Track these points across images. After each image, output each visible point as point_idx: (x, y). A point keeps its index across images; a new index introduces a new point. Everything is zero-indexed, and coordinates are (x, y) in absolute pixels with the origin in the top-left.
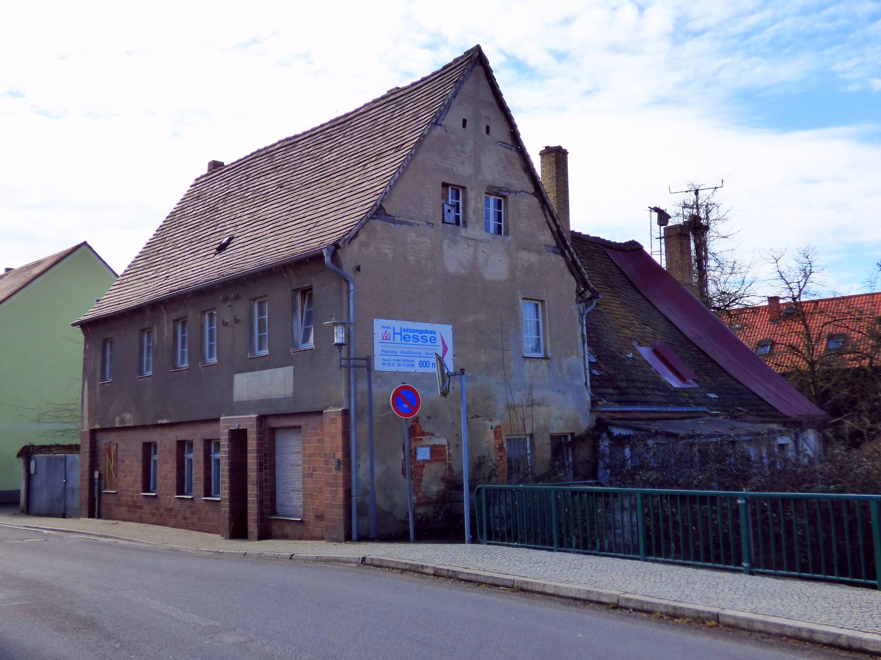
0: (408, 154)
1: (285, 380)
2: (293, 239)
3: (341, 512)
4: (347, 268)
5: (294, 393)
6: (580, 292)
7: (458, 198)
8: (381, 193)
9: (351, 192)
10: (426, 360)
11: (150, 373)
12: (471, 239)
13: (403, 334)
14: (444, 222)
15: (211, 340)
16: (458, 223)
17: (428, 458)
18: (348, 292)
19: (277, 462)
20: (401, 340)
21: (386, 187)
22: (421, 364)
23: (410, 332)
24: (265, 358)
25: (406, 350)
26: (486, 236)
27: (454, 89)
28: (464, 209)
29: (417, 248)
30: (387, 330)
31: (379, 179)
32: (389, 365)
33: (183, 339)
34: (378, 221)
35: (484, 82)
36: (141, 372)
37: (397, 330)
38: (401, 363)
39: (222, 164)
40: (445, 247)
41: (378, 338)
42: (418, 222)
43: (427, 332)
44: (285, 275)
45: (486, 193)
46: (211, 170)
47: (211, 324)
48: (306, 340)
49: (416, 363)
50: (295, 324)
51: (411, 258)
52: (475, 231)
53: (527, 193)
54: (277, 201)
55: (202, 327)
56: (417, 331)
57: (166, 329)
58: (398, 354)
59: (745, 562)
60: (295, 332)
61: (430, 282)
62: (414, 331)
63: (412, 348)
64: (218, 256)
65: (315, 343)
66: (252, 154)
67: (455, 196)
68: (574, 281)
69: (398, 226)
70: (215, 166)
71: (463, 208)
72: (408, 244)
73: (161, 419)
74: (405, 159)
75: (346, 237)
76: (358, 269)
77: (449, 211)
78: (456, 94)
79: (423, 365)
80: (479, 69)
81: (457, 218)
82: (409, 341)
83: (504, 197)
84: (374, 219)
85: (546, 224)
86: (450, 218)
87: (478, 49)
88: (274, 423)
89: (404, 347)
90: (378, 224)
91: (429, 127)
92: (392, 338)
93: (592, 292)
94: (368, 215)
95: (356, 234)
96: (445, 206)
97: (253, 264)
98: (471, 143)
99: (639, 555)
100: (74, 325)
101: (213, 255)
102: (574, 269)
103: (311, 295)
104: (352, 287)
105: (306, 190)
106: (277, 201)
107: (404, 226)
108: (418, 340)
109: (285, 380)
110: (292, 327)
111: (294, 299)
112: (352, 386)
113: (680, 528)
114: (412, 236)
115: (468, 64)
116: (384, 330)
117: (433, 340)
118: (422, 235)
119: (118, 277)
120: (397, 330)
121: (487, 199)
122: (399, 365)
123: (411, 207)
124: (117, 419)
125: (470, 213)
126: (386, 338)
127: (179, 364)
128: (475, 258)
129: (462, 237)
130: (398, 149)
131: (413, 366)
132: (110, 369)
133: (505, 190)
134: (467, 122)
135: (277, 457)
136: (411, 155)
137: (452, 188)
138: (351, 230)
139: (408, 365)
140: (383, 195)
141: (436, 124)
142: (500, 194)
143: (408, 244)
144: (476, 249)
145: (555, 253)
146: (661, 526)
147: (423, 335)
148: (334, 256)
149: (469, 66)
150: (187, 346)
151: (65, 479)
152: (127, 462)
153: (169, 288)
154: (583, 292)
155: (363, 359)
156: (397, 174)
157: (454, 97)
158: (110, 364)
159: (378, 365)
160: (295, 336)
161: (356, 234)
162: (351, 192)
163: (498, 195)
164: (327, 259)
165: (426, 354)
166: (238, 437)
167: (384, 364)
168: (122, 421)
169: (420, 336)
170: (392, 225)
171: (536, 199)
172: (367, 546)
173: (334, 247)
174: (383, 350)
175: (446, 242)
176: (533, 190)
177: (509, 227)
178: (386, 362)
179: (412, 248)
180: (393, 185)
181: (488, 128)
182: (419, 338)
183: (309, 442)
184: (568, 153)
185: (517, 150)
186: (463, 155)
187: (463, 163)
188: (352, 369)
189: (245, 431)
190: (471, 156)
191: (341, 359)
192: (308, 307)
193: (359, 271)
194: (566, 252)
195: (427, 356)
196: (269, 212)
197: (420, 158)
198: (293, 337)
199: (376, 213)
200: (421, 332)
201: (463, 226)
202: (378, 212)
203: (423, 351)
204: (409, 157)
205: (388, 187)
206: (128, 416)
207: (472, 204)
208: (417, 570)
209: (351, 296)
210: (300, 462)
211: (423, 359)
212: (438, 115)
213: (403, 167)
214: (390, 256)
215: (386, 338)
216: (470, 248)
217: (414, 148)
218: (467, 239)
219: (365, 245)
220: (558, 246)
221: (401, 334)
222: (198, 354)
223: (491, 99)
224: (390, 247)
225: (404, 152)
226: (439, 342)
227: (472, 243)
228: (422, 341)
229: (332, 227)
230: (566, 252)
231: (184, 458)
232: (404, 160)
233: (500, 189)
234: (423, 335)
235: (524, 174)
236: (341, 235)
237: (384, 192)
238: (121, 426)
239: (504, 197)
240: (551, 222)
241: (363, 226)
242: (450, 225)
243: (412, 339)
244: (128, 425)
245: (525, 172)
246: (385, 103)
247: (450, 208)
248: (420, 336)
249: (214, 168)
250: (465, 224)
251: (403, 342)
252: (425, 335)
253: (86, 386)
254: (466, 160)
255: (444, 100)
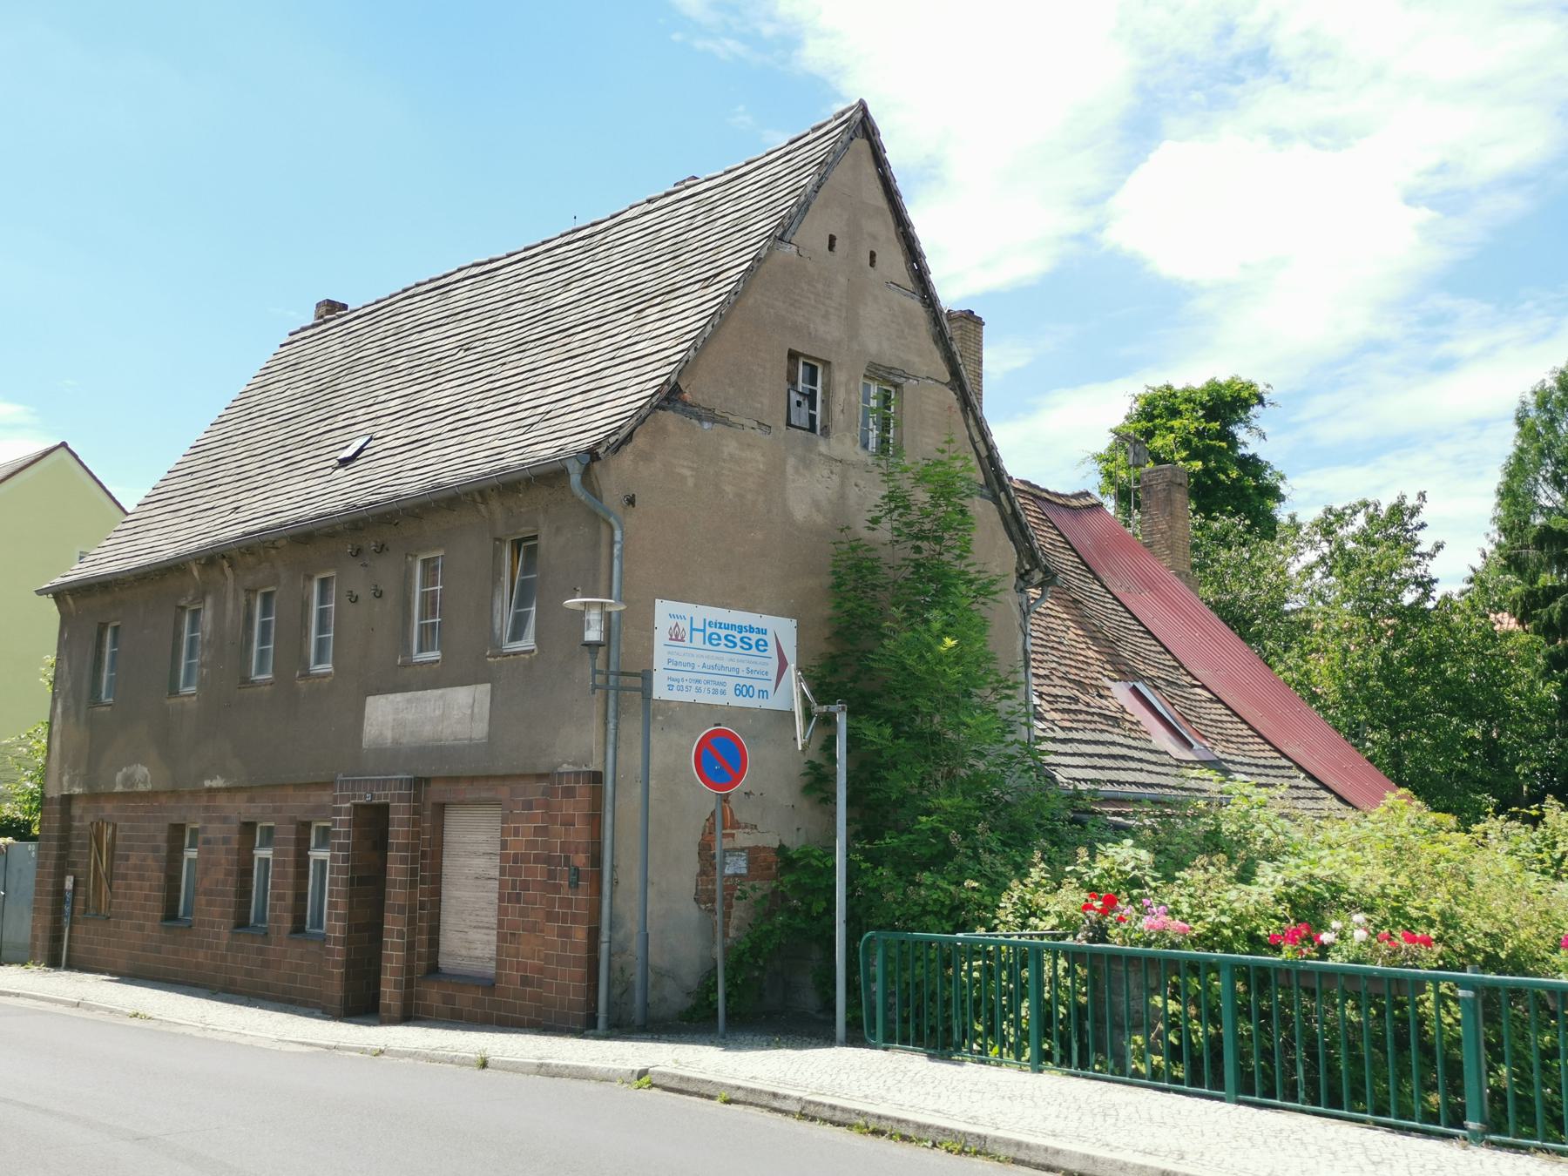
0: (730, 291)
1: (473, 711)
2: (497, 443)
3: (581, 970)
4: (612, 497)
5: (490, 735)
6: (1023, 571)
7: (814, 382)
8: (680, 361)
9: (613, 358)
10: (748, 682)
11: (192, 689)
12: (836, 460)
13: (709, 630)
14: (789, 424)
15: (322, 628)
16: (812, 429)
17: (744, 871)
18: (612, 543)
19: (445, 871)
20: (704, 643)
21: (688, 349)
22: (740, 691)
23: (720, 627)
24: (435, 666)
25: (713, 663)
26: (863, 455)
27: (817, 177)
28: (826, 403)
29: (738, 469)
30: (680, 622)
31: (671, 335)
32: (680, 689)
33: (265, 627)
34: (670, 413)
35: (870, 169)
36: (174, 691)
37: (698, 624)
38: (702, 686)
39: (345, 307)
40: (789, 470)
41: (661, 637)
42: (744, 421)
43: (751, 630)
44: (482, 507)
45: (865, 376)
46: (322, 317)
47: (323, 599)
48: (517, 635)
49: (730, 689)
50: (498, 605)
51: (728, 488)
52: (843, 445)
53: (936, 381)
54: (461, 374)
55: (306, 605)
56: (733, 627)
57: (230, 605)
58: (696, 669)
59: (1471, 1120)
60: (498, 620)
61: (759, 536)
62: (727, 627)
63: (722, 659)
64: (341, 472)
65: (538, 639)
66: (405, 290)
67: (807, 377)
68: (1014, 550)
69: (706, 425)
70: (331, 308)
71: (823, 401)
72: (724, 461)
73: (212, 778)
74: (724, 300)
75: (612, 440)
76: (631, 501)
77: (799, 404)
78: (819, 187)
79: (741, 692)
80: (861, 144)
81: (812, 418)
82: (718, 644)
83: (897, 386)
84: (663, 409)
85: (969, 441)
86: (801, 417)
87: (862, 106)
88: (436, 792)
89: (708, 657)
90: (670, 418)
91: (769, 243)
92: (687, 638)
93: (1044, 573)
94: (653, 400)
95: (629, 437)
96: (793, 394)
97: (418, 485)
98: (842, 280)
99: (1223, 1090)
100: (40, 592)
101: (330, 470)
102: (1014, 528)
103: (532, 552)
104: (618, 536)
105: (520, 356)
106: (461, 374)
107: (718, 427)
108: (735, 645)
109: (473, 711)
110: (492, 610)
111: (497, 554)
112: (611, 726)
113: (1412, 1041)
114: (730, 447)
115: (843, 131)
116: (672, 623)
117: (761, 645)
118: (749, 445)
119: (127, 514)
120: (698, 624)
121: (866, 387)
122: (698, 690)
123: (731, 391)
124: (119, 776)
125: (836, 409)
126: (676, 636)
127: (253, 673)
128: (843, 496)
129: (820, 454)
130: (707, 282)
131: (723, 693)
132: (110, 679)
133: (899, 372)
134: (837, 242)
135: (446, 862)
136: (736, 293)
137: (804, 363)
138: (621, 427)
139: (715, 692)
140: (682, 364)
141: (781, 239)
142: (887, 378)
143: (724, 461)
144: (844, 478)
145: (982, 496)
146: (1388, 1027)
147: (744, 634)
148: (586, 473)
149: (845, 137)
150: (272, 637)
151: (4, 891)
152: (132, 861)
153: (239, 530)
154: (1027, 572)
155: (636, 675)
156: (709, 328)
157: (816, 192)
158: (112, 669)
159: (660, 691)
160: (497, 626)
161: (629, 437)
162: (613, 358)
163: (886, 381)
164: (575, 478)
165: (749, 671)
166: (372, 822)
167: (670, 687)
168: (128, 779)
169: (739, 636)
170: (695, 422)
171: (952, 393)
172: (368, 1041)
173: (588, 456)
174: (669, 661)
175: (791, 461)
176: (948, 378)
177: (904, 442)
178: (675, 684)
179: (730, 470)
180: (702, 345)
181: (873, 255)
182: (737, 640)
183: (517, 832)
184: (984, 324)
185: (923, 301)
186: (827, 302)
187: (826, 316)
188: (612, 692)
189: (383, 810)
190: (841, 304)
191: (595, 672)
192: (525, 571)
193: (634, 506)
194: (1002, 495)
195: (749, 675)
196: (446, 393)
197: (751, 301)
198: (492, 629)
199: (667, 399)
200: (740, 629)
201: (821, 434)
202: (670, 397)
203: (743, 667)
204: (733, 298)
205: (692, 351)
206: (142, 771)
207: (840, 395)
208: (770, 1102)
209: (616, 552)
210: (496, 873)
211: (742, 682)
212: (786, 221)
213: (721, 315)
214: (690, 482)
215: (677, 636)
216: (834, 477)
217: (742, 280)
218: (831, 459)
219: (645, 457)
220: (988, 484)
221: (704, 631)
222: (293, 658)
223: (882, 202)
224: (691, 464)
225: (724, 287)
226: (772, 650)
227: (837, 468)
228: (742, 647)
229: (579, 422)
230: (1002, 495)
231: (253, 856)
232: (722, 302)
233: (890, 370)
234: (744, 634)
235: (933, 346)
236: (602, 435)
237: (686, 359)
238: (126, 790)
239: (897, 386)
240: (977, 438)
241: (642, 421)
242: (799, 431)
243: (723, 641)
244: (141, 788)
245: (936, 343)
246: (674, 203)
247: (800, 398)
248: (739, 636)
249: (328, 312)
250: (826, 431)
251: (708, 646)
252: (748, 634)
253: (59, 710)
254: (832, 310)
255: (799, 195)
